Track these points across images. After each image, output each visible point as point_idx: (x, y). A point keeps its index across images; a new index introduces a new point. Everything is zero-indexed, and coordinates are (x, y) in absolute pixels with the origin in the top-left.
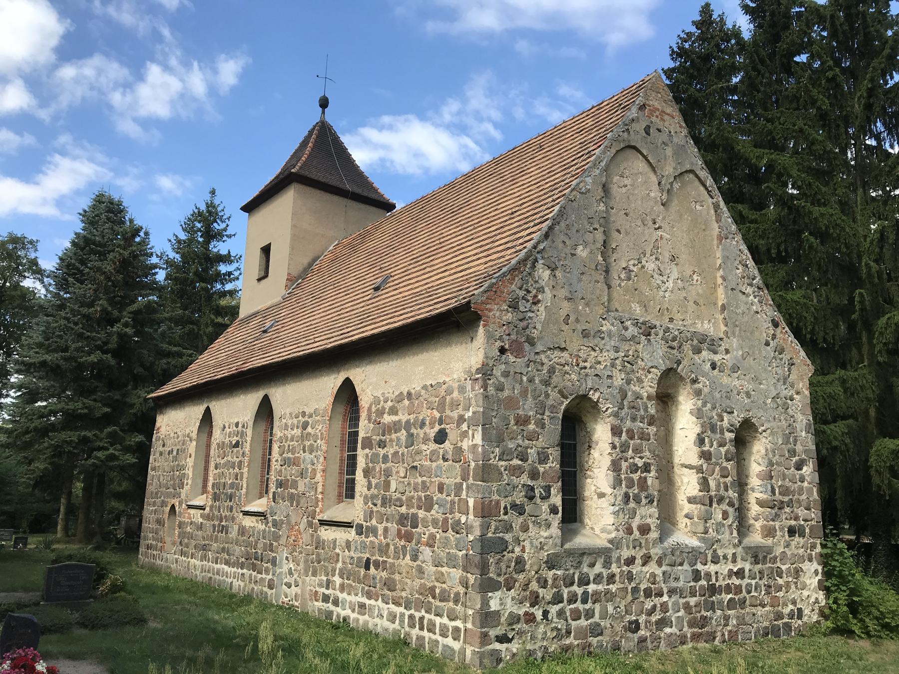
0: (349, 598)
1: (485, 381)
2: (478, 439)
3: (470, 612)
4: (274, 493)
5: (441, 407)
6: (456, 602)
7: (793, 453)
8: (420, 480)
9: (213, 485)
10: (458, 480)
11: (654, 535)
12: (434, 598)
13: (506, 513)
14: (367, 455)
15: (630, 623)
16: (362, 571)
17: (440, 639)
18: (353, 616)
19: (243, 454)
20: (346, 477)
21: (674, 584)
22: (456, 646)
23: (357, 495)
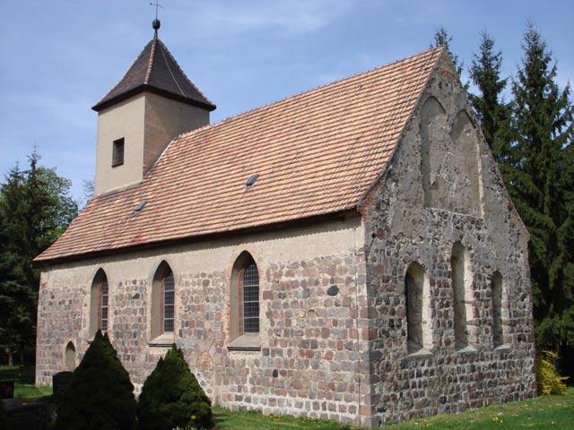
0: (260, 396)
1: (367, 256)
2: (364, 291)
3: (363, 396)
4: (180, 331)
5: (332, 271)
6: (352, 390)
7: (520, 290)
8: (317, 319)
9: (114, 326)
10: (349, 317)
11: (452, 345)
12: (333, 390)
13: (380, 336)
14: (269, 303)
15: (442, 398)
16: (271, 379)
17: (339, 414)
18: (264, 407)
19: (145, 303)
20: (165, 319)
21: (462, 374)
22: (353, 416)
23: (261, 329)
